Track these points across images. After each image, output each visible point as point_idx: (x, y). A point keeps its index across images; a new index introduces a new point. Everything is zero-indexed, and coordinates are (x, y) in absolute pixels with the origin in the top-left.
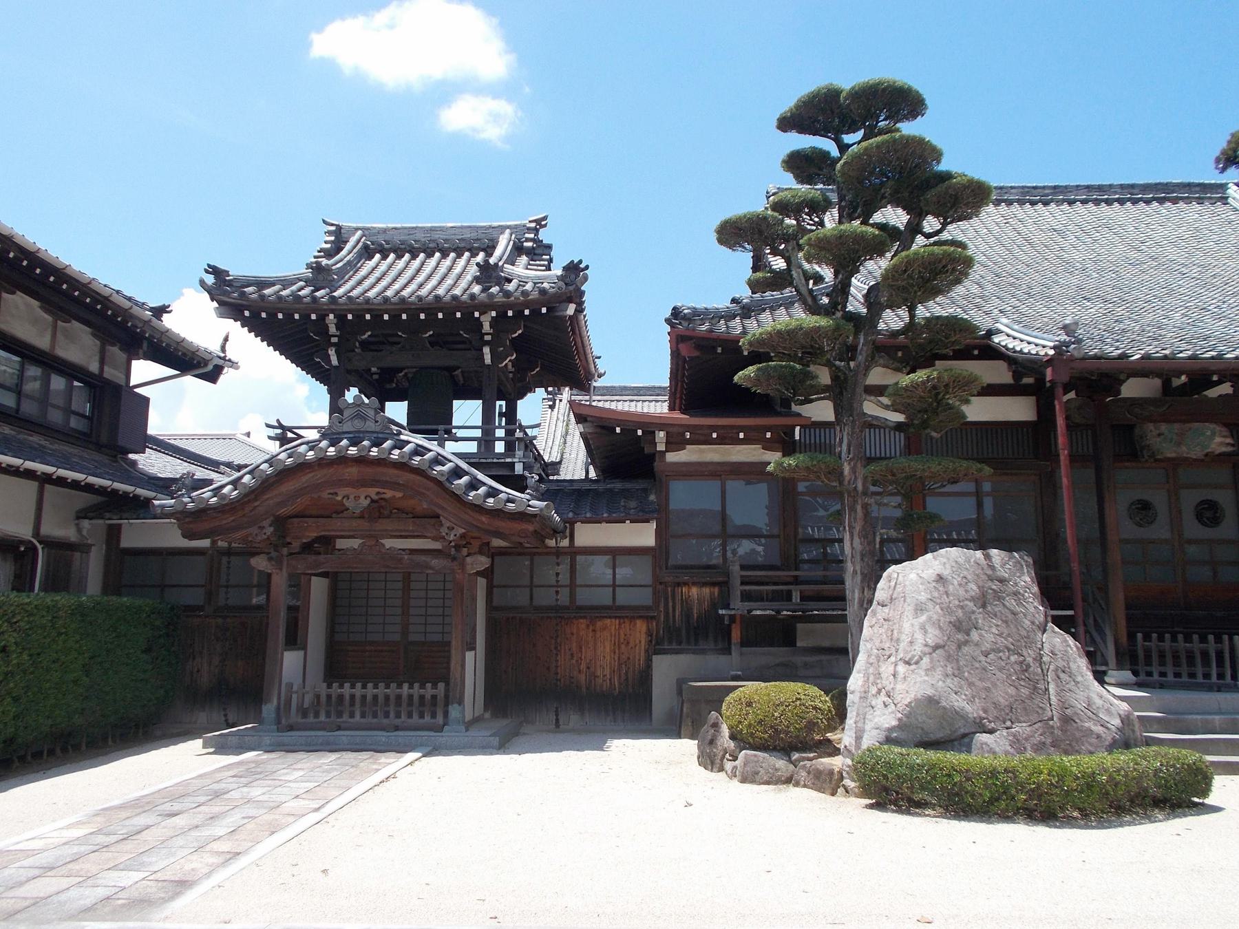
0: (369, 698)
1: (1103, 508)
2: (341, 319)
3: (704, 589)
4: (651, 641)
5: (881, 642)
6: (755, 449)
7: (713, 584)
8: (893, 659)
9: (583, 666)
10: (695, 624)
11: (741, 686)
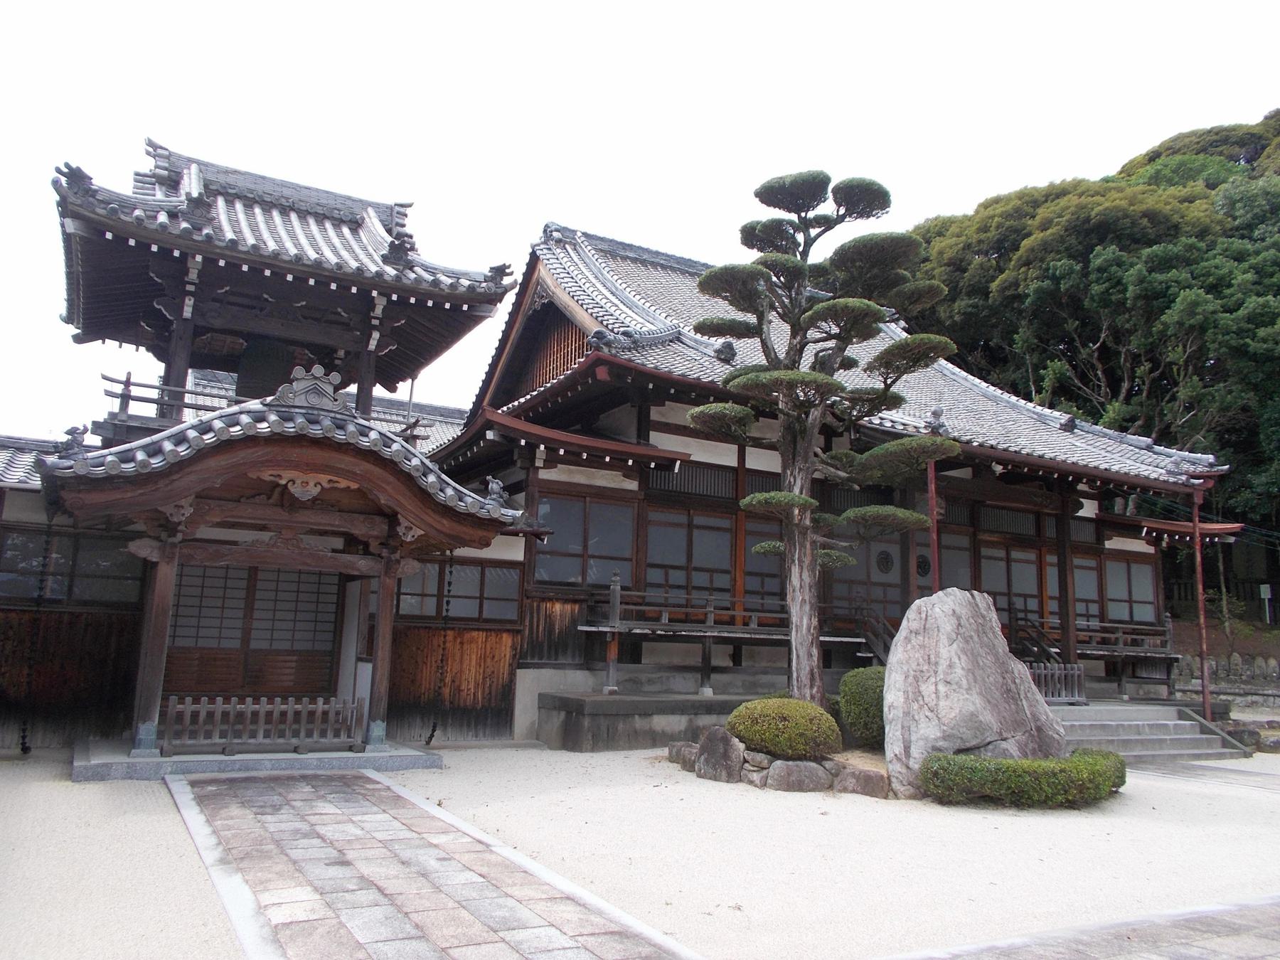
0: (276, 715)
1: (908, 562)
2: (210, 262)
3: (566, 606)
4: (515, 655)
5: (918, 665)
6: (616, 476)
7: (575, 601)
8: (933, 680)
9: (448, 680)
10: (556, 640)
11: (748, 701)
